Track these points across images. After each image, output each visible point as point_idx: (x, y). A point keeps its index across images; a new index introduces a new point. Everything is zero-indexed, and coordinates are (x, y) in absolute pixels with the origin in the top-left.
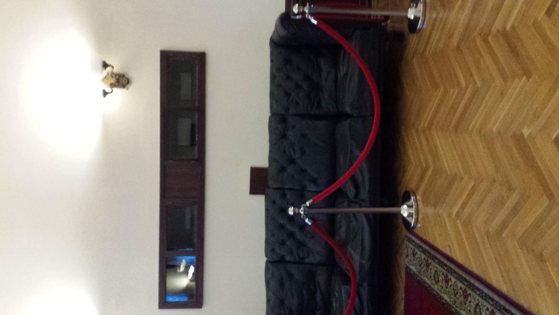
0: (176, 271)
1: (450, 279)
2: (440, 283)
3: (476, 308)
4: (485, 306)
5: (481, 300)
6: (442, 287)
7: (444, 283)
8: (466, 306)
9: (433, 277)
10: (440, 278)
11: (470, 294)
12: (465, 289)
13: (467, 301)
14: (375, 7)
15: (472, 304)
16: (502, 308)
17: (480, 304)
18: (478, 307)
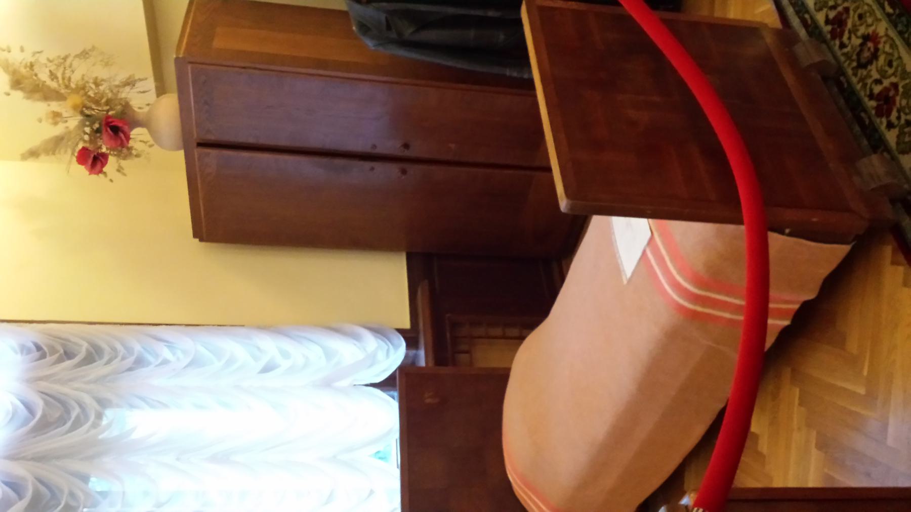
0: (250, 203)
1: (827, 22)
2: (862, 30)
3: (870, 62)
4: (844, 54)
5: (850, 72)
6: (861, 17)
7: (849, 24)
8: (893, 79)
9: (882, 60)
10: (857, 42)
11: (871, 96)
12: (834, 37)
13: (840, 14)
14: (501, 37)
15: (876, 76)
16: (810, 29)
17: (855, 64)
18: (863, 61)
